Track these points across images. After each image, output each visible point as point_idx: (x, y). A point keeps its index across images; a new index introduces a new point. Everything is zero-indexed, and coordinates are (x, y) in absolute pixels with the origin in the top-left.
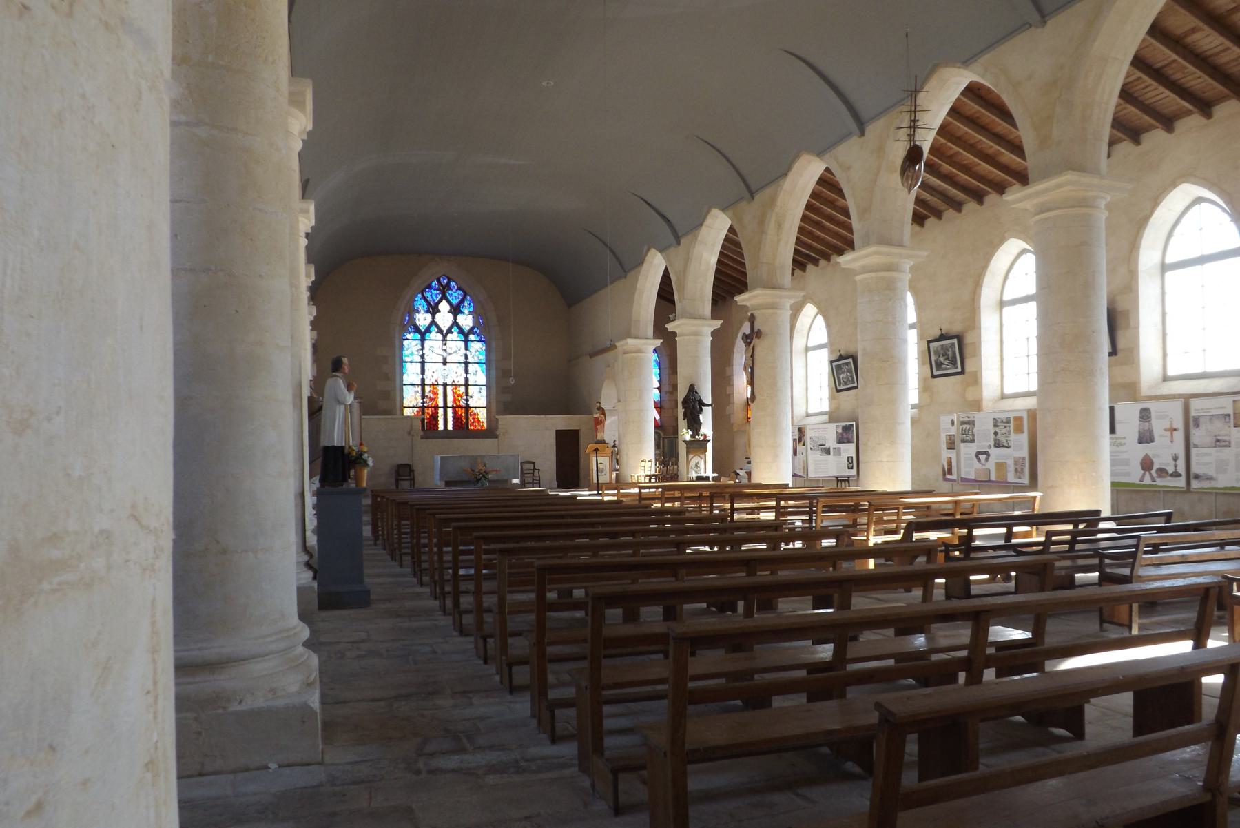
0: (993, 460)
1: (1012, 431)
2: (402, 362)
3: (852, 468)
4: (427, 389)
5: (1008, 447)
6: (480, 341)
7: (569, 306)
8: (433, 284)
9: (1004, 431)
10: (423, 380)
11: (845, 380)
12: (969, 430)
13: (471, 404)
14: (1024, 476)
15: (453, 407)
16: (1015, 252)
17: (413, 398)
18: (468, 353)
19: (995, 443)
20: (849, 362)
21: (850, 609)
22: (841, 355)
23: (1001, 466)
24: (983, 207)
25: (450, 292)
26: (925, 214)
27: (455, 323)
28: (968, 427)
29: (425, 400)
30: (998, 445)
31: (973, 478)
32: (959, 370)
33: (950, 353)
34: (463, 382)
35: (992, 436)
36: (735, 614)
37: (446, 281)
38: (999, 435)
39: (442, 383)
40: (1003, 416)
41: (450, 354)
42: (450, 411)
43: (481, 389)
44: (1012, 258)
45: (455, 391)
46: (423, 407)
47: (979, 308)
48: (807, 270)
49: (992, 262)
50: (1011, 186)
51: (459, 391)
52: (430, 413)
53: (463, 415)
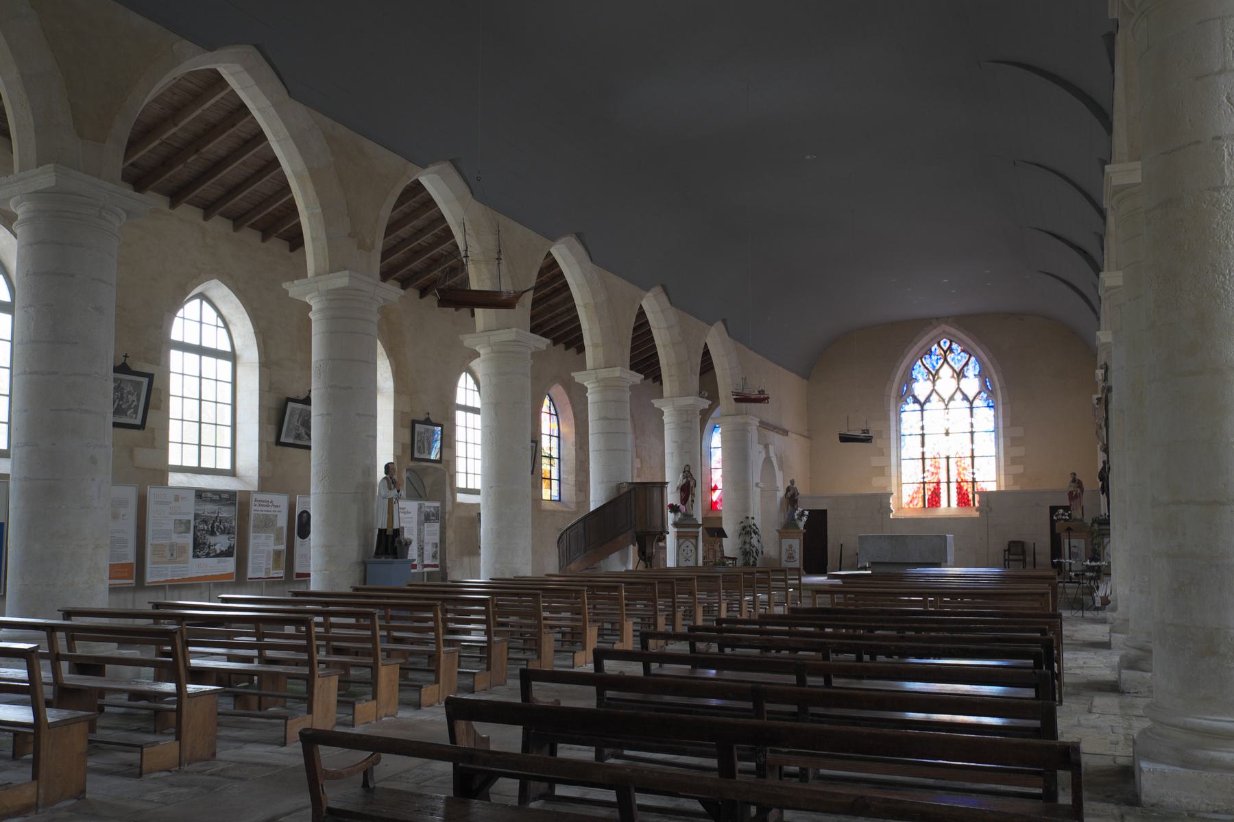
2: (899, 436)
4: (928, 462)
6: (988, 406)
8: (933, 349)
15: (957, 482)
25: (952, 355)
27: (959, 389)
29: (925, 475)
34: (969, 454)
37: (948, 344)
42: (953, 487)
46: (924, 483)
51: (964, 463)
52: (932, 489)
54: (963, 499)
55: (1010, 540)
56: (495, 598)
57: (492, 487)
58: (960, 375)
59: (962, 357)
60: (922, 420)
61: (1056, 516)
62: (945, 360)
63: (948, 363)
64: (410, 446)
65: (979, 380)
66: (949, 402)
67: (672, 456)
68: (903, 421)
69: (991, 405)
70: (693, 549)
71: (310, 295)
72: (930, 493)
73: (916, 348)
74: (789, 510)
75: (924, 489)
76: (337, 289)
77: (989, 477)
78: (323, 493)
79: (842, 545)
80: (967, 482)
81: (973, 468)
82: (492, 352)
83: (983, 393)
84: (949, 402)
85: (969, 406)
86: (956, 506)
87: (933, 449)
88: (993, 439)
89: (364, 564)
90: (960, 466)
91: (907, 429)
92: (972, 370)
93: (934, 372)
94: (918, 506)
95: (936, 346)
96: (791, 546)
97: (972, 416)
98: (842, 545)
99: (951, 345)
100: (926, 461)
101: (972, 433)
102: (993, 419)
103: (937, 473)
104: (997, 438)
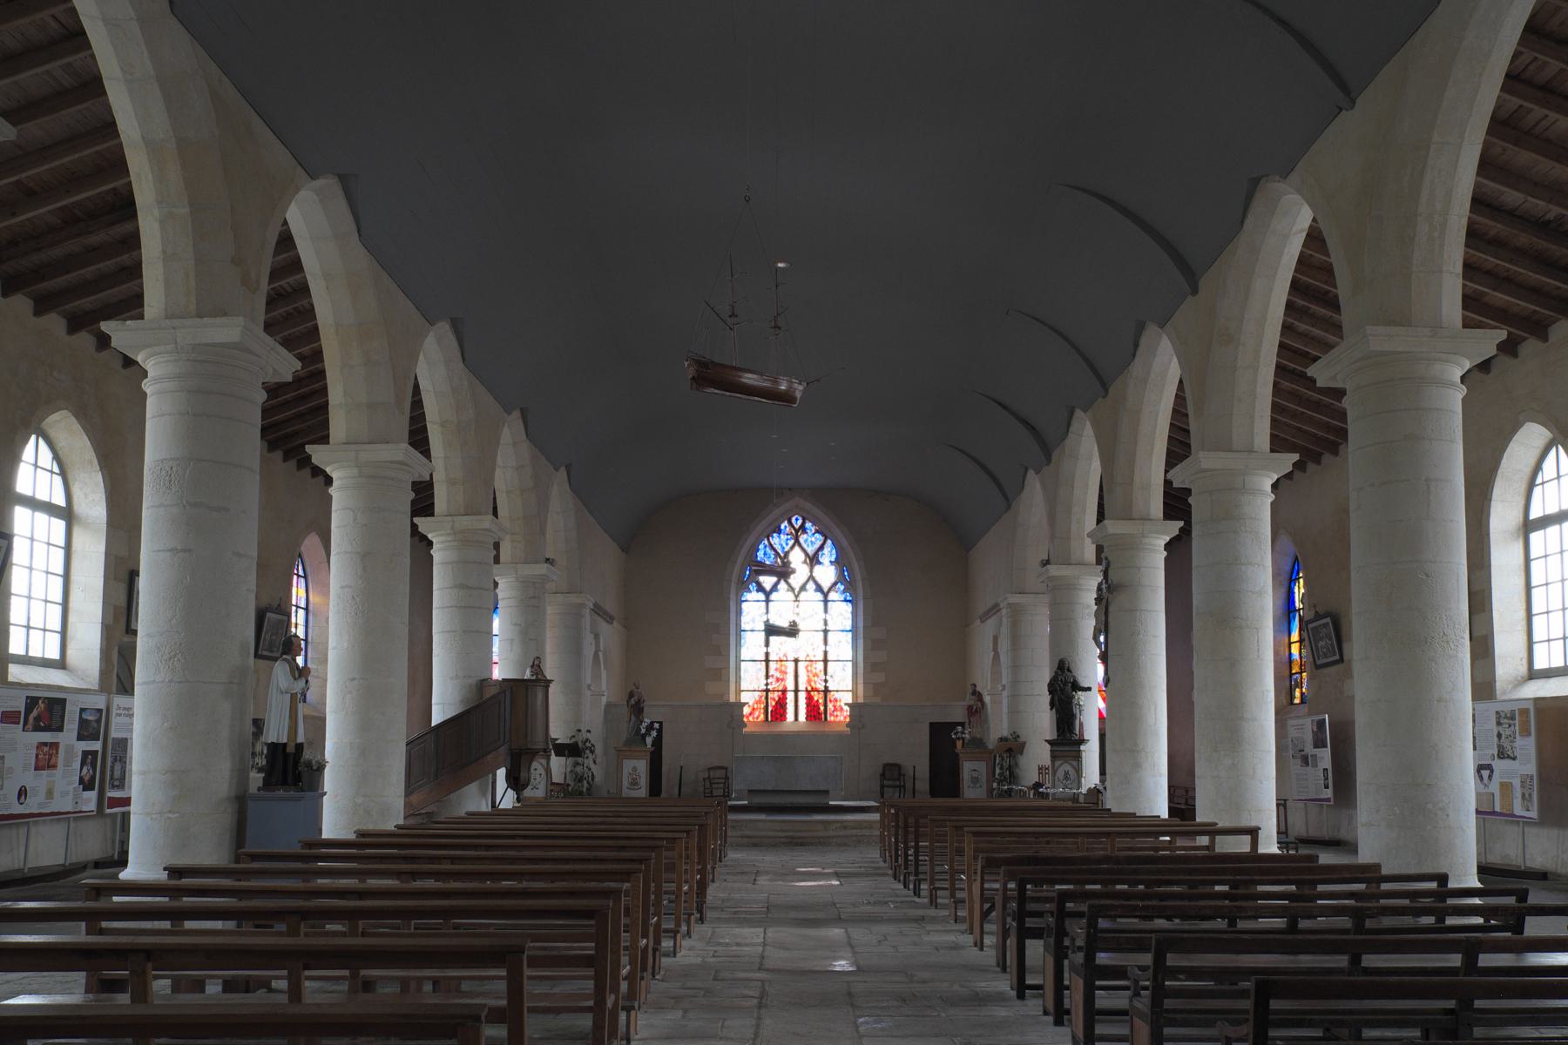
1: (1517, 733)
2: (739, 631)
4: (772, 666)
6: (846, 600)
8: (782, 527)
10: (767, 654)
11: (1324, 650)
13: (831, 686)
14: (1532, 805)
15: (807, 690)
17: (754, 678)
18: (828, 617)
20: (1328, 623)
25: (805, 536)
27: (811, 578)
29: (769, 681)
30: (1502, 754)
34: (821, 657)
35: (1496, 739)
36: (1130, 1011)
37: (800, 522)
39: (792, 659)
41: (804, 619)
42: (802, 696)
43: (845, 665)
44: (1536, 453)
45: (809, 668)
46: (767, 691)
47: (1489, 534)
49: (1504, 461)
51: (816, 668)
52: (777, 699)
53: (821, 701)
54: (814, 712)
55: (885, 762)
56: (1109, 853)
57: (353, 679)
58: (813, 560)
59: (816, 539)
60: (767, 612)
61: (955, 734)
62: (797, 541)
63: (800, 545)
64: (125, 612)
65: (836, 569)
66: (799, 592)
67: (511, 644)
68: (744, 614)
69: (848, 598)
70: (543, 772)
71: (148, 350)
72: (774, 703)
73: (765, 523)
74: (632, 723)
75: (767, 698)
76: (214, 345)
77: (843, 683)
78: (170, 681)
79: (682, 767)
80: (818, 691)
81: (826, 674)
82: (360, 476)
83: (839, 584)
84: (799, 592)
85: (822, 599)
86: (805, 720)
87: (779, 649)
88: (850, 641)
89: (241, 801)
90: (811, 671)
91: (748, 623)
92: (828, 554)
93: (782, 555)
94: (759, 720)
95: (786, 523)
96: (635, 769)
97: (826, 611)
98: (682, 767)
99: (804, 523)
100: (771, 664)
101: (826, 632)
102: (850, 616)
103: (782, 680)
104: (854, 639)
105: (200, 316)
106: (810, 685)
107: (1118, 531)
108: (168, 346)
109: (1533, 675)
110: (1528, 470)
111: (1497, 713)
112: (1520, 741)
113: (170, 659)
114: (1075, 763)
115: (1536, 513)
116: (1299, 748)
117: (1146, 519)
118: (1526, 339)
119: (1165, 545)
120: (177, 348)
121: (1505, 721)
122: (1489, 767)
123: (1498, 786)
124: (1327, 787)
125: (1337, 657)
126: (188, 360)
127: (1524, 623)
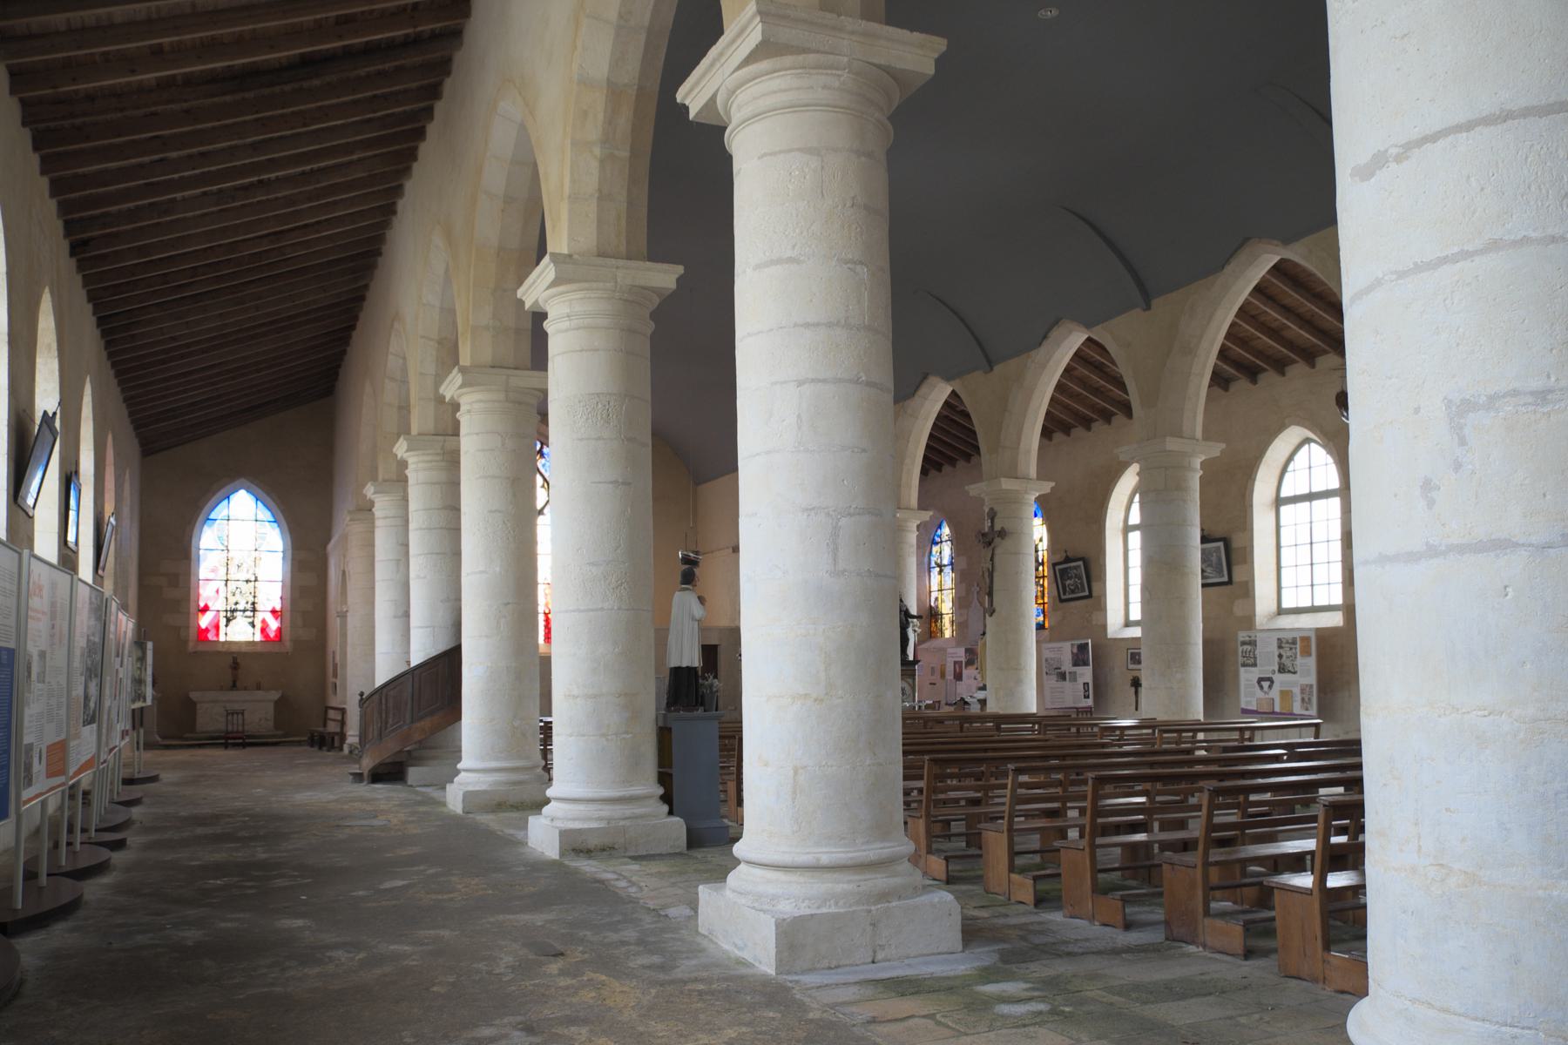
0: (1277, 687)
3: (1088, 697)
5: (1295, 673)
7: (697, 484)
9: (1289, 653)
11: (1072, 588)
12: (1250, 652)
15: (545, 613)
16: (1296, 441)
19: (1280, 668)
20: (1079, 566)
21: (13, 650)
22: (1067, 557)
23: (1286, 695)
24: (1257, 386)
25: (543, 461)
26: (1070, 423)
28: (1249, 648)
31: (1255, 708)
32: (1226, 579)
33: (1214, 559)
35: (1277, 659)
38: (1284, 658)
40: (1289, 636)
44: (1291, 448)
47: (1252, 506)
48: (957, 467)
50: (1237, 380)
78: (619, 609)
99: (542, 448)
105: (629, 258)
106: (548, 608)
107: (1009, 488)
108: (608, 284)
109: (1281, 611)
110: (1283, 460)
111: (1278, 639)
112: (1300, 660)
113: (617, 588)
114: (910, 681)
115: (1285, 493)
116: (1055, 667)
117: (1027, 478)
118: (1297, 362)
119: (1036, 498)
120: (616, 287)
121: (1287, 645)
122: (1270, 680)
123: (1278, 694)
124: (1087, 697)
125: (1087, 593)
126: (620, 299)
127: (1275, 573)
